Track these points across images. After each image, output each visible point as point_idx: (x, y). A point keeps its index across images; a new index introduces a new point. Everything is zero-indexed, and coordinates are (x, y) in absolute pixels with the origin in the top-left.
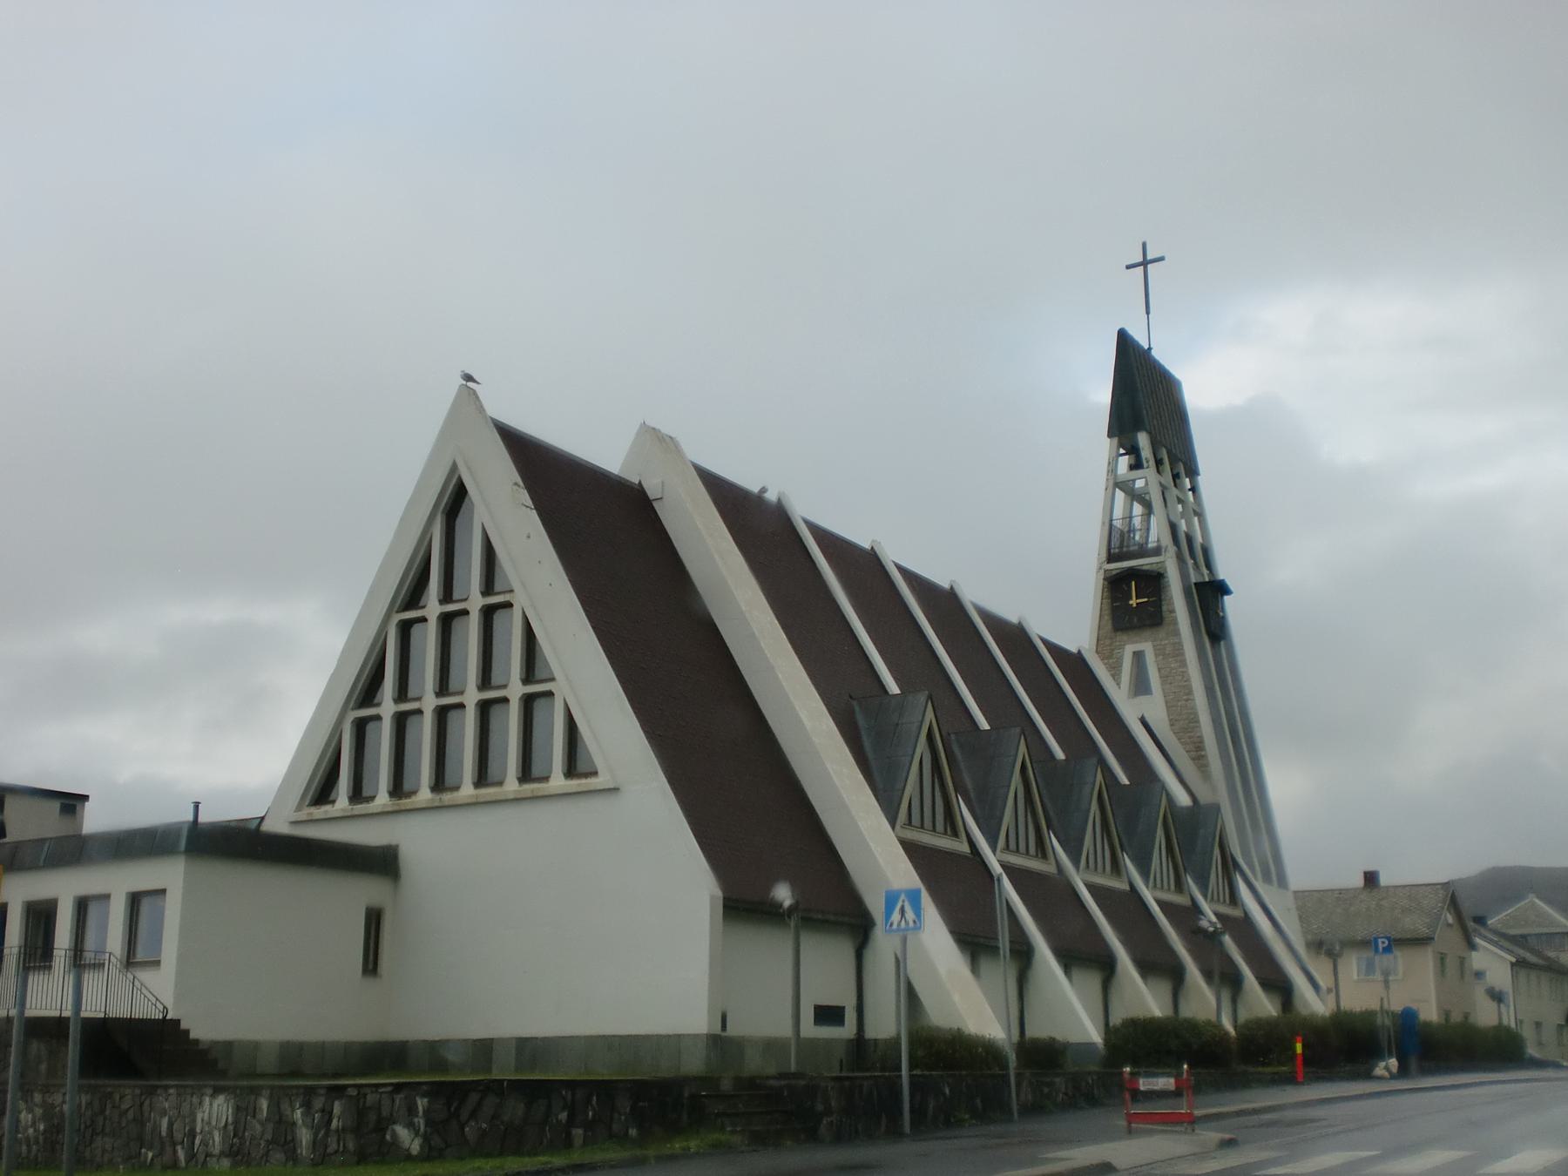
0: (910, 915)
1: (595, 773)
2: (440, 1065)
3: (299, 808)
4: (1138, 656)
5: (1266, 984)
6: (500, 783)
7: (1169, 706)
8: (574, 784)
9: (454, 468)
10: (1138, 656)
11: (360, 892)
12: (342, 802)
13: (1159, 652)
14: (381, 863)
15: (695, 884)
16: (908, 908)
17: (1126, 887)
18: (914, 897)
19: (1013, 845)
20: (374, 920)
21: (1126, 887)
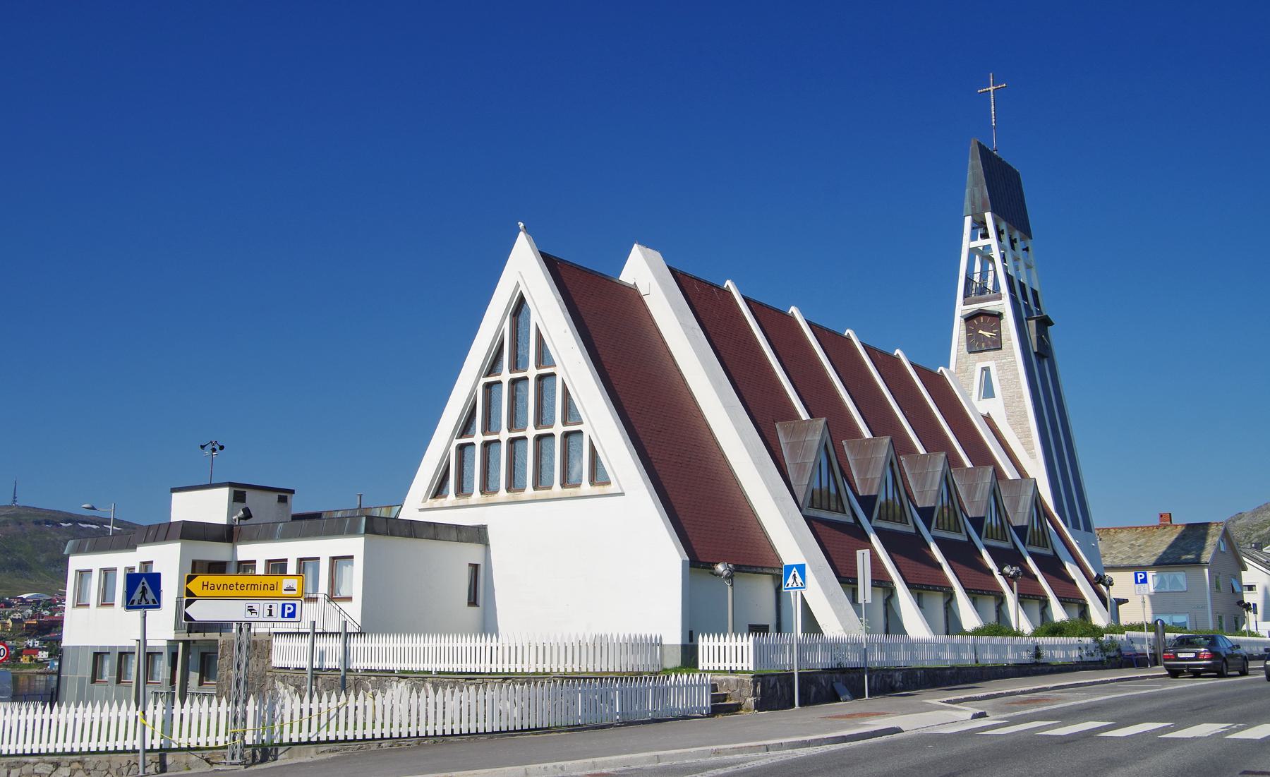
0: (799, 580)
1: (609, 483)
2: (1119, 650)
3: (424, 501)
4: (986, 370)
5: (1064, 602)
6: (550, 488)
7: (1007, 407)
8: (597, 490)
9: (518, 285)
10: (986, 370)
11: (472, 552)
12: (451, 497)
13: (1000, 368)
14: (478, 535)
15: (665, 556)
16: (797, 575)
17: (913, 530)
18: (801, 568)
19: (825, 504)
20: (475, 568)
21: (913, 530)
